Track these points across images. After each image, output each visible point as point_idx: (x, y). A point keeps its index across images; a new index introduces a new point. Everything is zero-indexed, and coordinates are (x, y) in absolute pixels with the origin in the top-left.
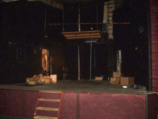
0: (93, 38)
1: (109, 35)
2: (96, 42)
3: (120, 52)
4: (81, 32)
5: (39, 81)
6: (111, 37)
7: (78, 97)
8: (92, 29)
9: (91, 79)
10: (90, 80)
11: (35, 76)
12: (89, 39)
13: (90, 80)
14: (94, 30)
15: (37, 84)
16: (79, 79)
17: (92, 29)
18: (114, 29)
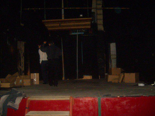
0: (79, 29)
1: (98, 26)
2: (83, 34)
3: (113, 47)
4: (66, 20)
5: (15, 83)
6: (101, 27)
7: (77, 101)
8: (81, 15)
9: (79, 78)
10: (77, 79)
11: (9, 76)
12: (75, 30)
13: (77, 79)
14: (85, 18)
15: (12, 86)
16: (64, 78)
17: (81, 15)
18: (104, 19)
